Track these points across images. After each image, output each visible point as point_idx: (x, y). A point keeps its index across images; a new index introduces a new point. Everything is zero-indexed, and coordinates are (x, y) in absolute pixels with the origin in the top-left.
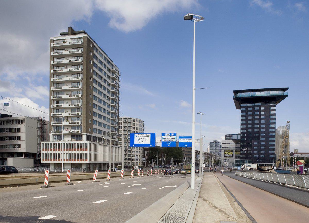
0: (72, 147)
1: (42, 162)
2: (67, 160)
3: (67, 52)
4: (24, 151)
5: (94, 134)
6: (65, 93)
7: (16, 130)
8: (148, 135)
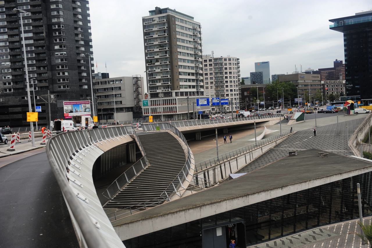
6: (155, 33)
7: (117, 88)
8: (205, 99)
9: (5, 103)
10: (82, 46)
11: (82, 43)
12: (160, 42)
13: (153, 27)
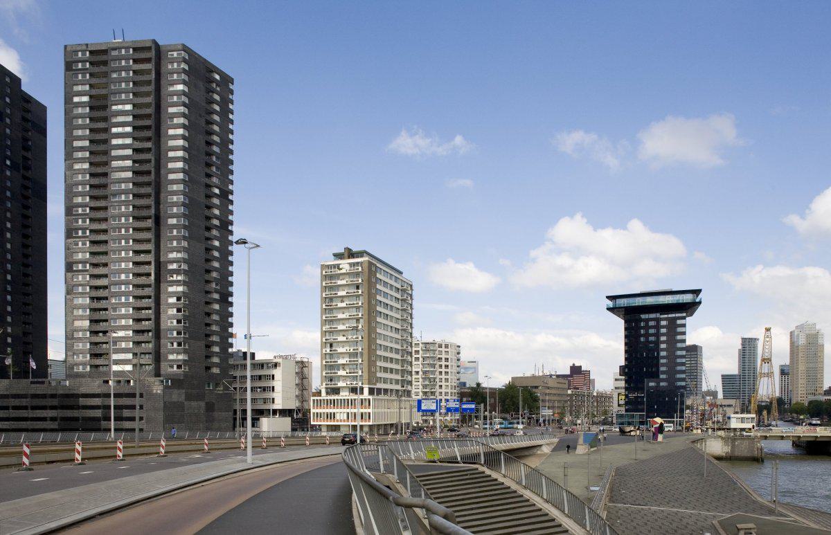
0: (352, 403)
1: (312, 423)
2: (344, 421)
3: (344, 282)
4: (280, 407)
5: (379, 386)
9: (75, 390)
10: (216, 301)
11: (216, 296)
12: (348, 325)
13: (338, 290)
